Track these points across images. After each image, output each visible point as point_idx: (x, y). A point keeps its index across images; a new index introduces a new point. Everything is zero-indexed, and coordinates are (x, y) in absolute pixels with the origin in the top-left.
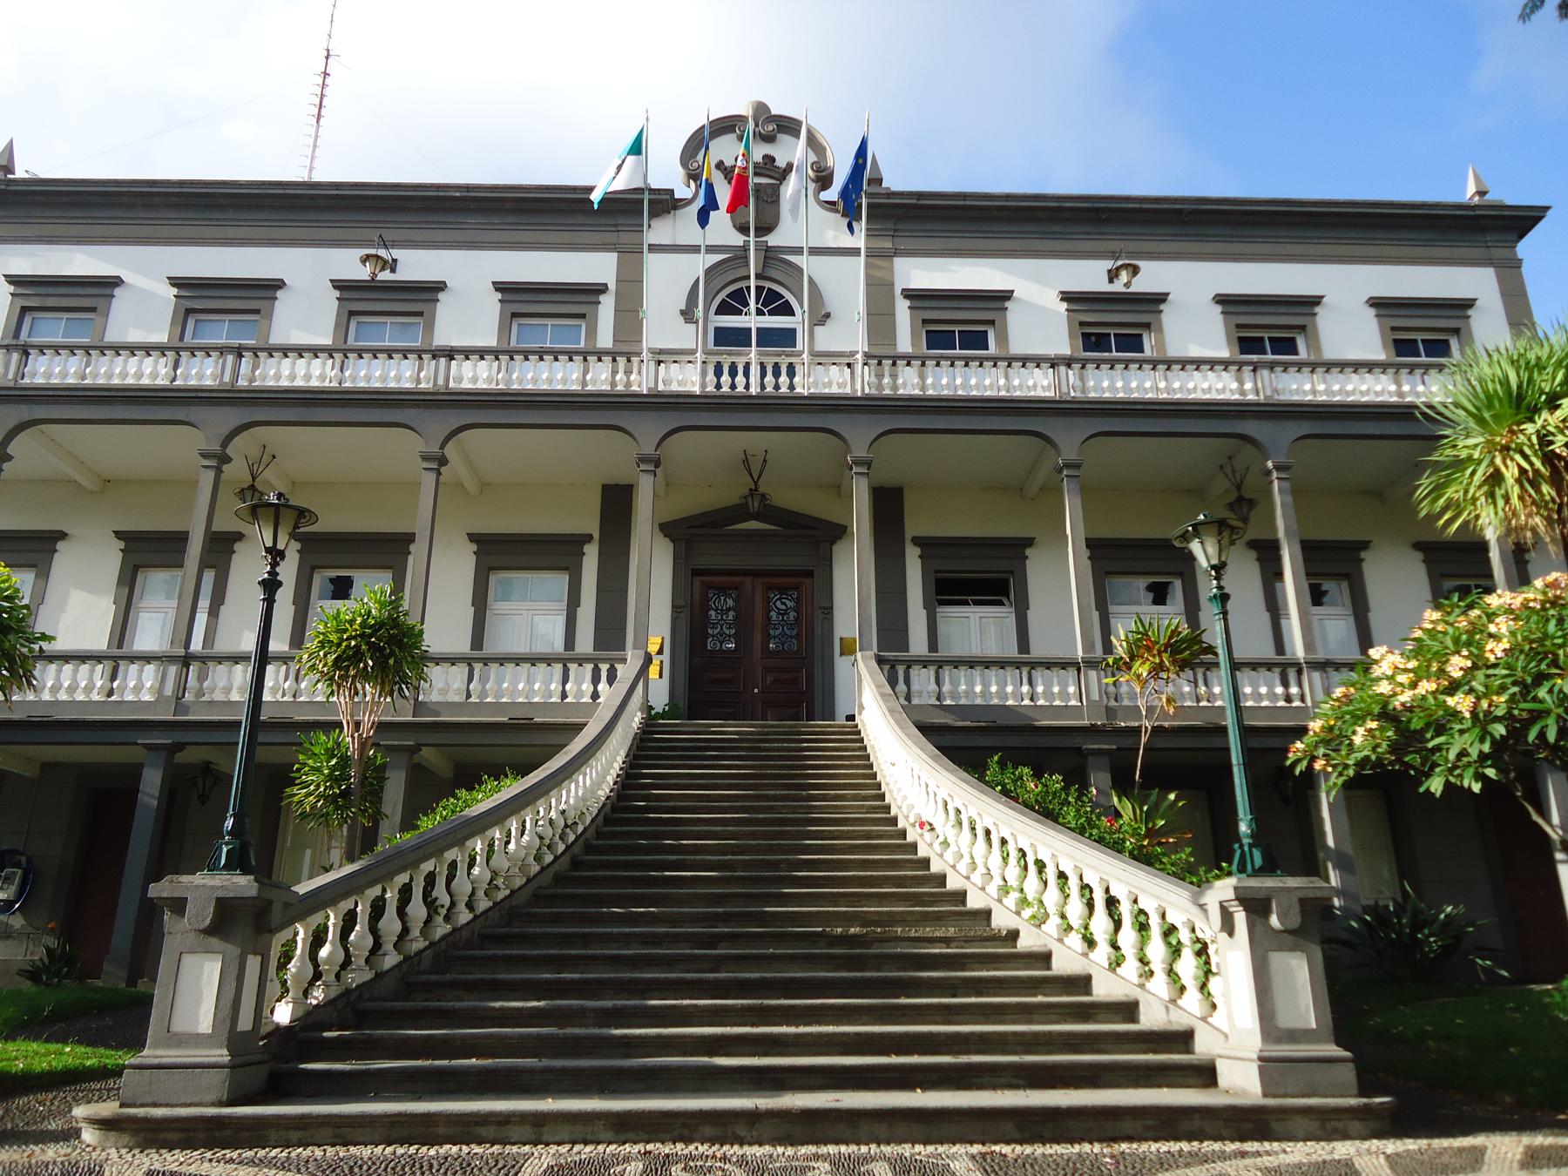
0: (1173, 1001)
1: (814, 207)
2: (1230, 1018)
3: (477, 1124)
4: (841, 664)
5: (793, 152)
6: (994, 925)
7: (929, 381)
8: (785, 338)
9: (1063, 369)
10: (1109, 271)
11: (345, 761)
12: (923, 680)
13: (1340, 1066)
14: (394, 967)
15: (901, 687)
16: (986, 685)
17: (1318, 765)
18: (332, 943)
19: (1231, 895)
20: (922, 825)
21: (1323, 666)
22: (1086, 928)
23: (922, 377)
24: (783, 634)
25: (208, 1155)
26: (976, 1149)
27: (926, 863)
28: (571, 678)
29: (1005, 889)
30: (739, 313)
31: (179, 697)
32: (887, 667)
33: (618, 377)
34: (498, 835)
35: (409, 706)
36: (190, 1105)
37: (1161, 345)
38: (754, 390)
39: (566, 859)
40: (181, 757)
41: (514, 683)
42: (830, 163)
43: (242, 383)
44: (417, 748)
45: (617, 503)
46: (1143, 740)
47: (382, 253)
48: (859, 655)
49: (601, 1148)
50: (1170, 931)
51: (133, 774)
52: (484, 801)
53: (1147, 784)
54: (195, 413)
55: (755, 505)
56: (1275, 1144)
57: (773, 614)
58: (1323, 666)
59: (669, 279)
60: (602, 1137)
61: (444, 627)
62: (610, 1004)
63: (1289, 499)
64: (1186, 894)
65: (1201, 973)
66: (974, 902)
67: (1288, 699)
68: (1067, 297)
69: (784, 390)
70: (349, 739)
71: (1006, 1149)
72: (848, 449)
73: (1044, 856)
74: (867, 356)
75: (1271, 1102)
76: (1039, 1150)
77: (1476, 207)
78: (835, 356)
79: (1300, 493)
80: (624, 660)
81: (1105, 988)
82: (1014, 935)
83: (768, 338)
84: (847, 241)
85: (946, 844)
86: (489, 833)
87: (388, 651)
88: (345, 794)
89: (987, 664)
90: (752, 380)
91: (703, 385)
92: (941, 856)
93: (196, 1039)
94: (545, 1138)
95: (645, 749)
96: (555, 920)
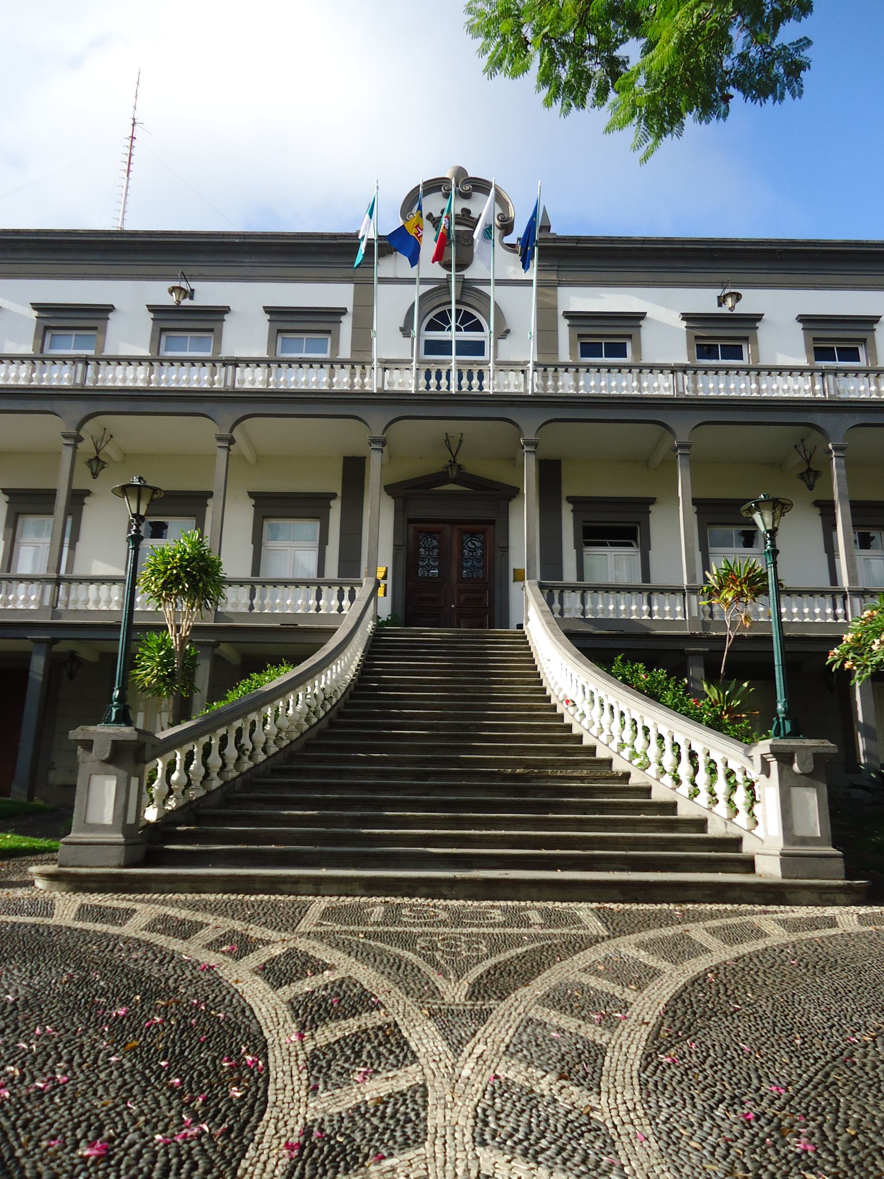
0: (730, 819)
2: (766, 830)
3: (279, 882)
4: (514, 588)
5: (484, 209)
6: (614, 769)
7: (581, 383)
8: (477, 348)
9: (680, 374)
10: (719, 297)
11: (170, 653)
12: (572, 601)
13: (833, 860)
14: (218, 788)
15: (557, 605)
16: (617, 605)
17: (847, 665)
18: (180, 771)
19: (767, 750)
20: (567, 702)
21: (862, 594)
23: (577, 380)
24: (473, 566)
25: (115, 896)
26: (594, 905)
27: (569, 727)
28: (324, 592)
29: (622, 746)
30: (443, 329)
32: (546, 591)
33: (356, 380)
34: (281, 704)
37: (756, 355)
38: (453, 390)
39: (325, 722)
40: (57, 648)
41: (283, 599)
42: (512, 215)
43: (89, 384)
44: (217, 644)
45: (354, 470)
46: (728, 645)
47: (183, 285)
48: (526, 582)
49: (357, 899)
50: (730, 774)
51: (25, 659)
52: (272, 679)
53: (729, 676)
54: (57, 406)
55: (453, 473)
56: (788, 908)
58: (862, 594)
59: (393, 303)
60: (357, 892)
61: (234, 561)
62: (359, 813)
63: (844, 472)
64: (741, 750)
65: (749, 801)
66: (602, 753)
67: (836, 617)
68: (686, 317)
69: (475, 390)
71: (613, 906)
72: (521, 433)
73: (649, 723)
74: (536, 365)
76: (634, 907)
78: (513, 364)
79: (851, 466)
80: (360, 585)
81: (685, 811)
82: (627, 776)
83: (465, 348)
84: (522, 275)
85: (583, 715)
87: (197, 576)
88: (171, 675)
89: (618, 589)
91: (417, 386)
92: (580, 723)
93: (103, 828)
94: (322, 892)
95: (375, 647)
96: (320, 760)
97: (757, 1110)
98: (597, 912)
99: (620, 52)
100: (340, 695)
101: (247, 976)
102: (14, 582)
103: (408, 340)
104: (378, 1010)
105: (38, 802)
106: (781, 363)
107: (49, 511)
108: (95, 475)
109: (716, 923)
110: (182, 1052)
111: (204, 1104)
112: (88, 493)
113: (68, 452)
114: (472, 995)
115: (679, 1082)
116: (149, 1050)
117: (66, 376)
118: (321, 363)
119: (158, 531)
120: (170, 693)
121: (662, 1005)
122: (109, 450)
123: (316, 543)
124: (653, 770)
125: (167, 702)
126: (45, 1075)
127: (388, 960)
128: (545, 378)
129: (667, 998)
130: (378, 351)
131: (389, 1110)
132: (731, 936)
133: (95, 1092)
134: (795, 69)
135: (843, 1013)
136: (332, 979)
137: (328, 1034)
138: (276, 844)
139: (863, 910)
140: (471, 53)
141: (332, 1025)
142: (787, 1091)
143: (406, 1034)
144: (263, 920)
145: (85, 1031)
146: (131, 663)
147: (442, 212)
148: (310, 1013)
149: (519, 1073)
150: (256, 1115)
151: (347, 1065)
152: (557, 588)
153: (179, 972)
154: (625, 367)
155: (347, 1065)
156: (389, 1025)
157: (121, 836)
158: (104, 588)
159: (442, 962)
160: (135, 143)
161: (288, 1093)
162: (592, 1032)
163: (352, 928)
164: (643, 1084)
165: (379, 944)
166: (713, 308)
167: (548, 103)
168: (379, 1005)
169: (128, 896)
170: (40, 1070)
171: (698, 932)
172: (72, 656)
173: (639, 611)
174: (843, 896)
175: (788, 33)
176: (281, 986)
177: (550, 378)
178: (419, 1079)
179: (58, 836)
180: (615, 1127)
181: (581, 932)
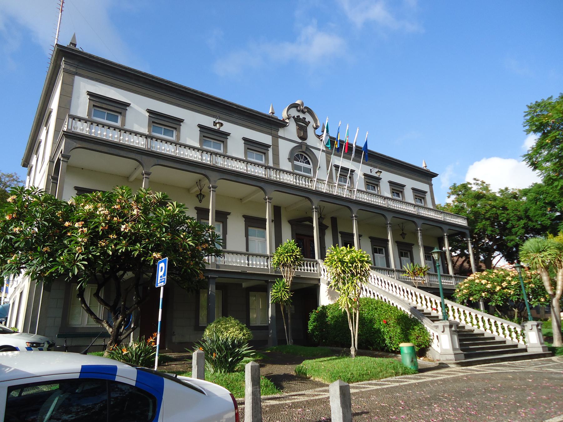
9: (149, 140)
77: (269, 117)
78: (321, 180)
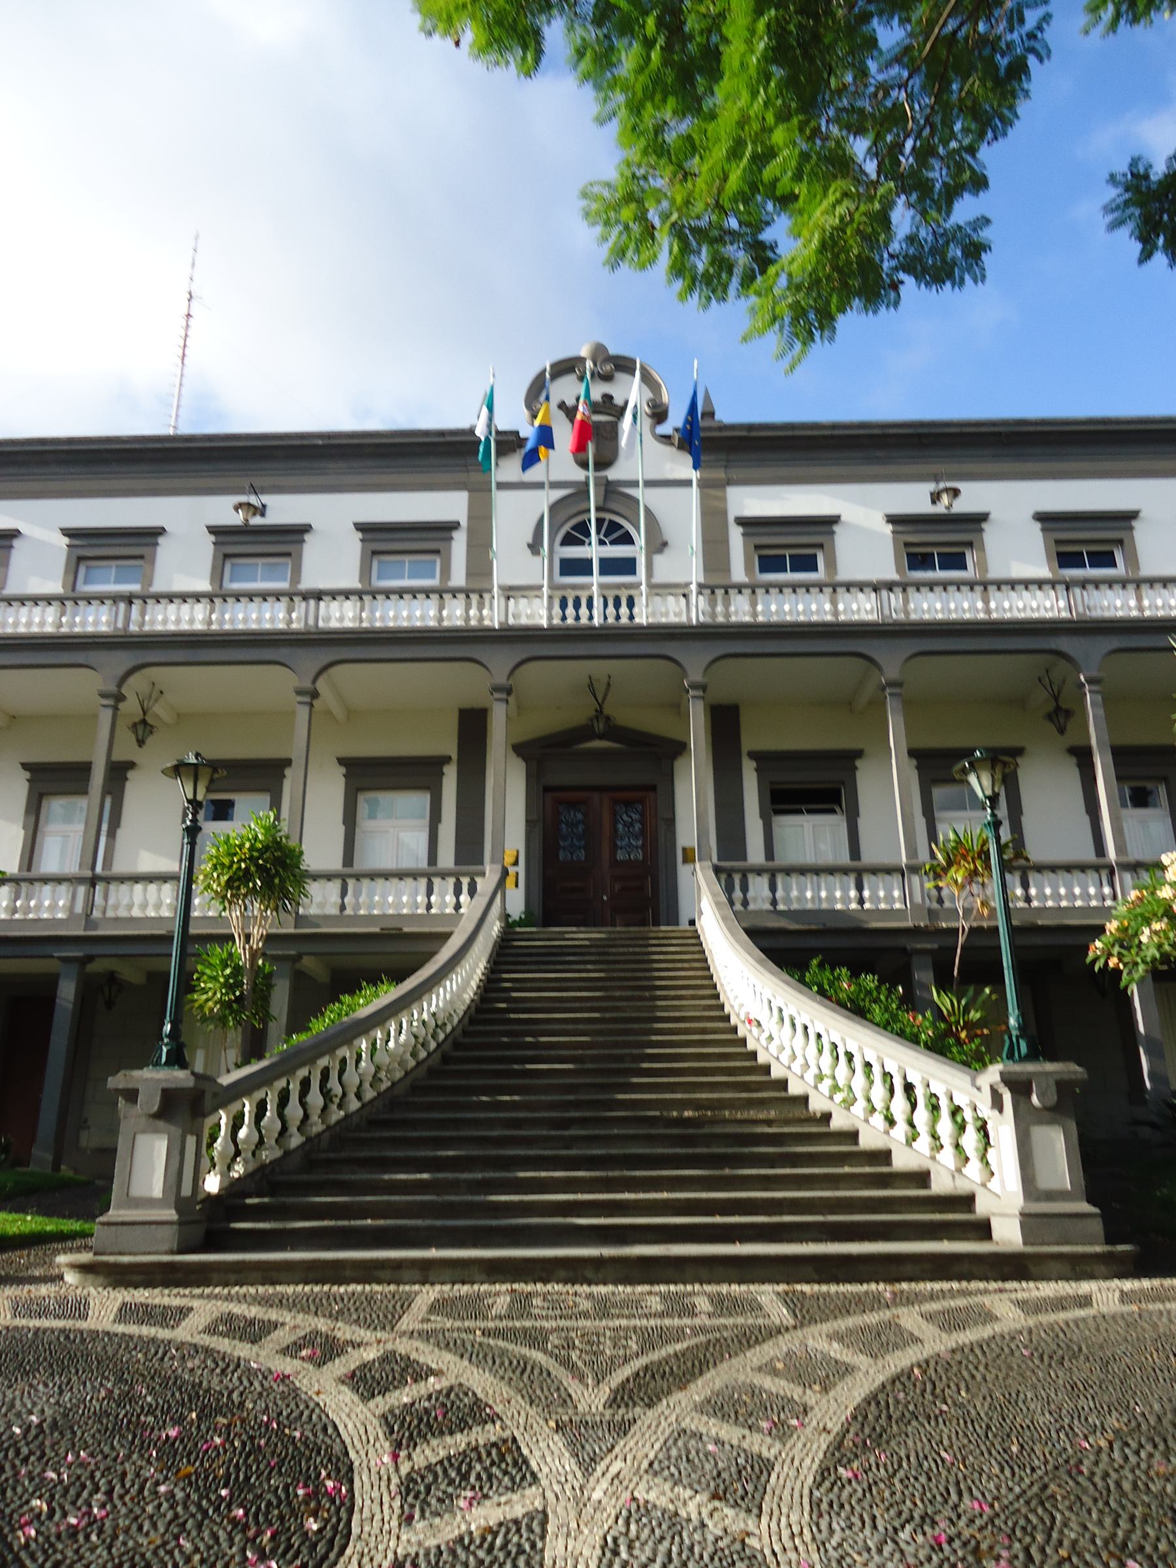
1: (650, 441)
4: (683, 871)
5: (632, 392)
7: (759, 608)
8: (627, 566)
9: (884, 593)
11: (237, 970)
15: (738, 894)
17: (1113, 962)
19: (998, 1078)
20: (750, 1022)
22: (888, 1109)
24: (630, 845)
25: (166, 1291)
26: (782, 1288)
28: (436, 885)
29: (820, 1077)
30: (582, 543)
31: (88, 915)
34: (379, 1035)
35: (291, 919)
36: (149, 1253)
37: (982, 565)
38: (596, 622)
39: (437, 1057)
40: (93, 967)
43: (133, 628)
44: (299, 957)
45: (473, 726)
47: (253, 500)
48: (698, 865)
49: (476, 1287)
50: (956, 1111)
51: (50, 983)
52: (368, 1003)
54: (93, 657)
55: (600, 727)
57: (620, 827)
59: (518, 513)
61: (320, 849)
62: (479, 1176)
63: (1101, 712)
64: (968, 1079)
65: (981, 1146)
68: (892, 519)
69: (624, 620)
70: (241, 951)
71: (806, 1288)
72: (685, 674)
74: (701, 586)
75: (1030, 1249)
76: (833, 1288)
78: (672, 586)
79: (1109, 702)
80: (483, 874)
81: (902, 1161)
82: (827, 1117)
83: (610, 566)
85: (771, 1038)
86: (372, 1033)
87: (272, 870)
88: (238, 1000)
90: (595, 612)
91: (550, 618)
93: (150, 1202)
95: (504, 955)
96: (431, 1107)
97: (952, 1531)
98: (785, 1298)
99: (766, 236)
100: (456, 1020)
101: (330, 1385)
102: (37, 884)
103: (538, 559)
104: (494, 1422)
105: (65, 1171)
106: (1016, 575)
107: (81, 789)
108: (141, 743)
109: (935, 1306)
110: (247, 1479)
111: (273, 1537)
112: (131, 765)
113: (106, 716)
114: (614, 1401)
115: (860, 1500)
116: (206, 1478)
117: (104, 619)
118: (427, 592)
119: (222, 811)
120: (238, 1023)
121: (851, 1408)
122: (159, 709)
123: (426, 821)
124: (859, 1108)
125: (235, 1036)
126: (79, 1509)
127: (511, 1363)
128: (713, 604)
129: (859, 1399)
130: (500, 575)
131: (498, 1542)
132: (951, 1322)
133: (140, 1528)
134: (975, 250)
135: (1077, 1413)
136: (438, 1387)
137: (427, 1454)
138: (373, 1218)
139: (1128, 1285)
140: (587, 241)
141: (434, 1442)
142: (992, 1506)
143: (525, 1451)
144: (355, 1317)
145: (128, 1457)
146: (187, 985)
147: (578, 399)
148: (406, 1430)
149: (664, 1493)
150: (336, 1550)
151: (450, 1490)
152: (737, 871)
153: (245, 1383)
154: (814, 585)
155: (450, 1490)
156: (505, 1441)
157: (173, 1212)
158: (152, 888)
159: (580, 1364)
160: (192, 322)
161: (377, 1523)
162: (759, 1444)
163: (467, 1324)
164: (815, 1504)
165: (501, 1343)
166: (924, 507)
167: (682, 297)
168: (493, 1418)
169: (182, 1291)
170: (74, 1503)
171: (910, 1319)
172: (111, 977)
173: (846, 899)
174: (1103, 1268)
175: (965, 210)
176: (373, 1396)
177: (719, 602)
178: (538, 1504)
179: (91, 1217)
180: (774, 1554)
181: (760, 1321)
